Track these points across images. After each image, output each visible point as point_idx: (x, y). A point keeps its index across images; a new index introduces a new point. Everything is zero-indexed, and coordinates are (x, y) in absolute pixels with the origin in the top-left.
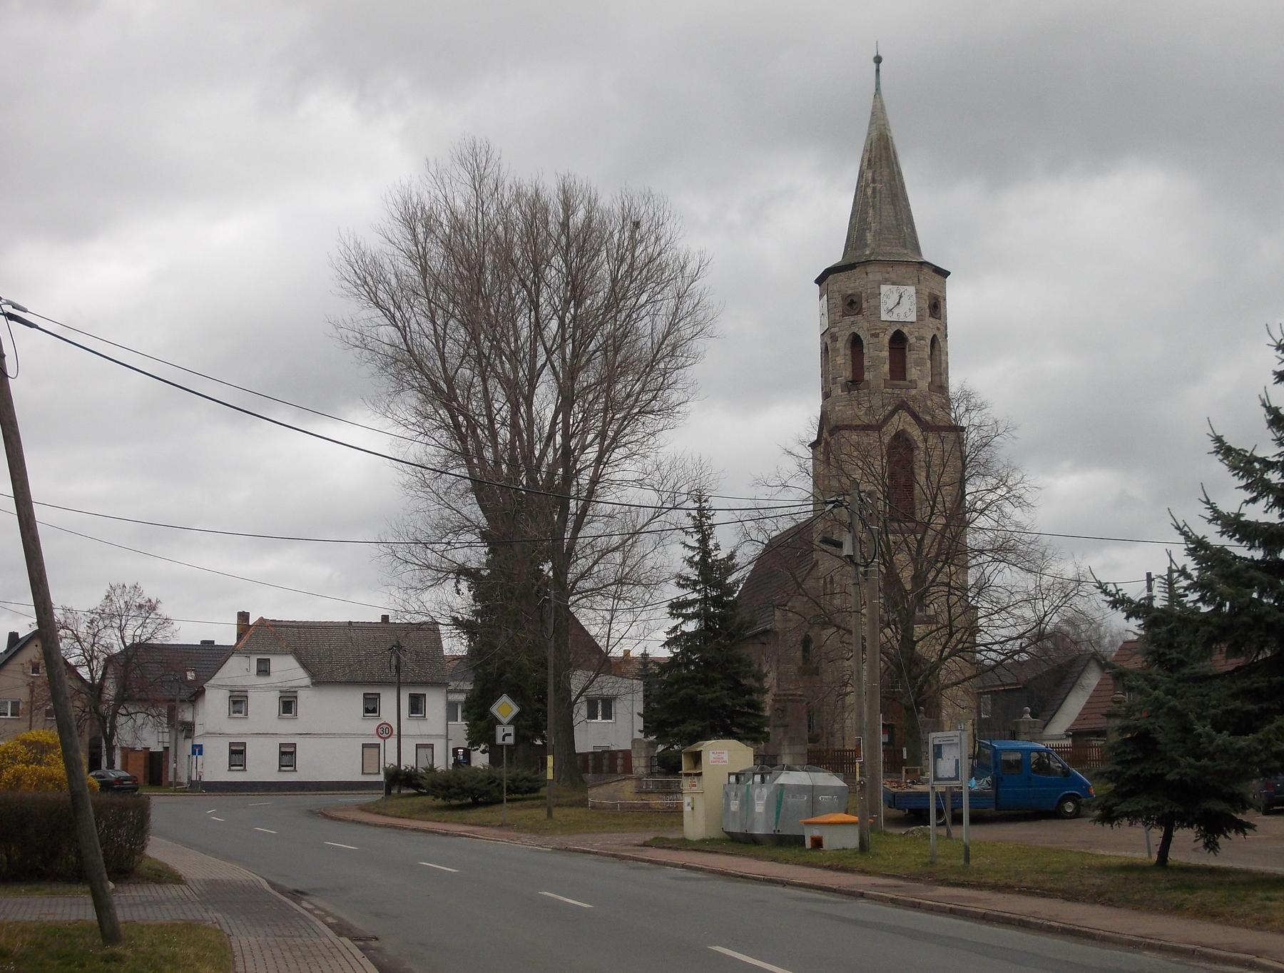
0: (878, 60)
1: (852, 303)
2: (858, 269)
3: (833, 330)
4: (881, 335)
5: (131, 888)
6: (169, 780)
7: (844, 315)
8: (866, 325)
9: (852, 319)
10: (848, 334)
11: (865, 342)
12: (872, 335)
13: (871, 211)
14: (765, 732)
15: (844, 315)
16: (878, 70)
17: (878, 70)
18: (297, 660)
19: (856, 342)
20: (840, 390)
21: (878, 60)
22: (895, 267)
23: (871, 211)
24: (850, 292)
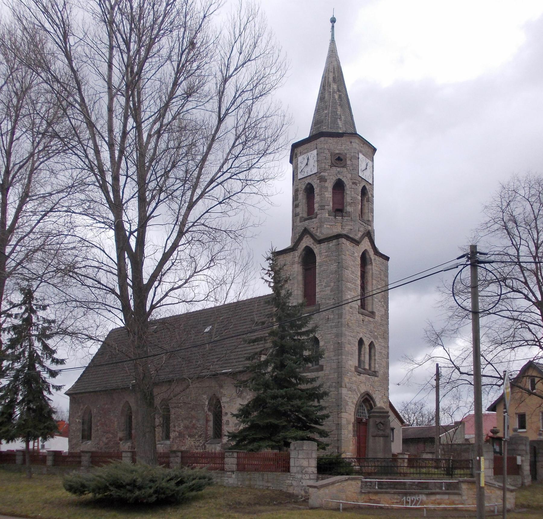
0: (333, 21)
1: (339, 159)
2: (344, 138)
3: (322, 174)
4: (358, 185)
5: (456, 473)
6: (21, 323)
7: (332, 165)
8: (349, 176)
9: (339, 169)
10: (335, 179)
11: (348, 186)
12: (354, 183)
13: (339, 108)
14: (69, 425)
15: (332, 165)
16: (333, 27)
17: (333, 27)
18: (293, 196)
19: (339, 186)
20: (327, 215)
21: (333, 21)
22: (364, 145)
23: (339, 108)
24: (337, 152)
